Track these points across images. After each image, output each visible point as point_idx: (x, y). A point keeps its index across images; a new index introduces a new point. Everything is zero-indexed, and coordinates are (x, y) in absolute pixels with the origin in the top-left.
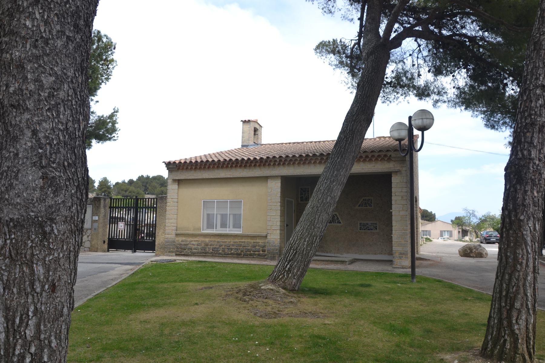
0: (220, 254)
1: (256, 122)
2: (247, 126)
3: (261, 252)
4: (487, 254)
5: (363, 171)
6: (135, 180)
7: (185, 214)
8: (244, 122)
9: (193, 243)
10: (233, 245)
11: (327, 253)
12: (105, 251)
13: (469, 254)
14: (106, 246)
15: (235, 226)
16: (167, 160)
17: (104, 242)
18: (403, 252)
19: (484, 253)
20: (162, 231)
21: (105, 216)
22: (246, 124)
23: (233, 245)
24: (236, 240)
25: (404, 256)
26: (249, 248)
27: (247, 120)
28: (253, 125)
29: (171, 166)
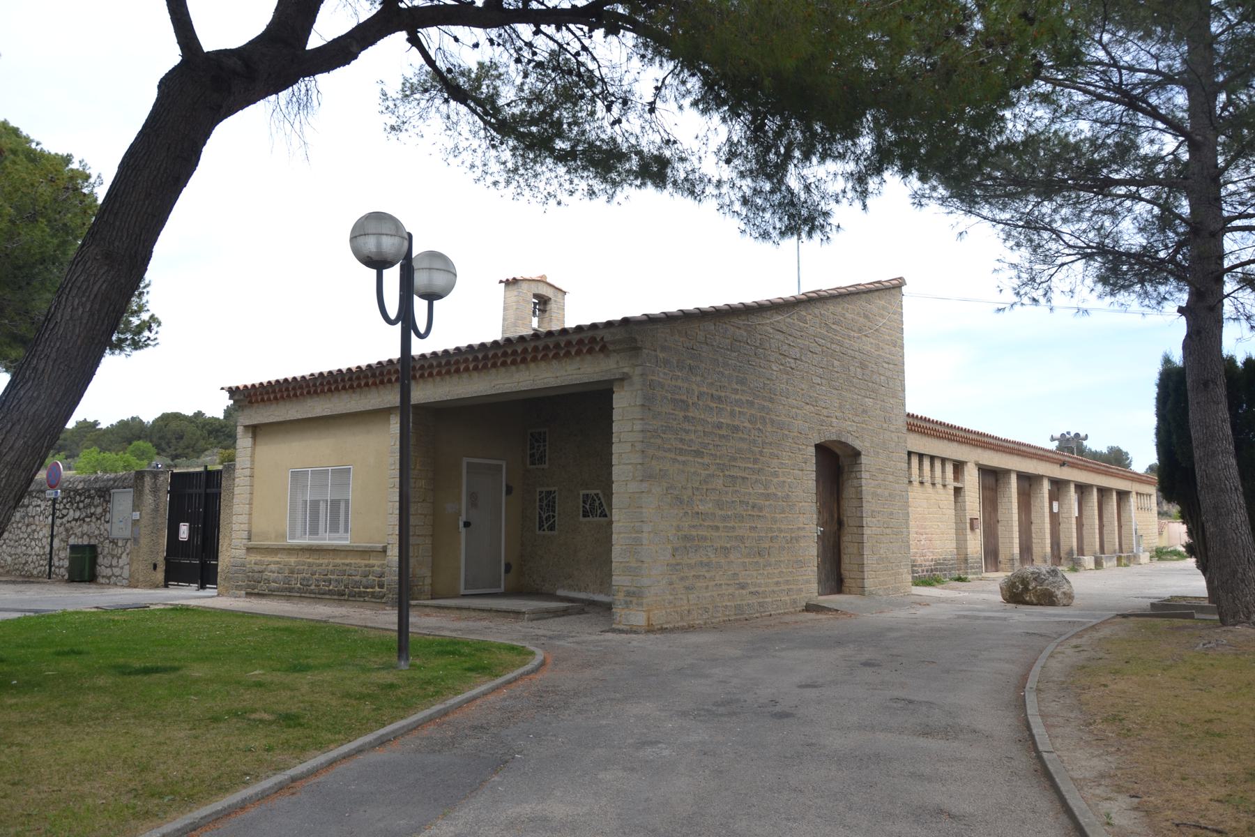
0: (312, 592)
1: (542, 281)
2: (513, 292)
3: (377, 589)
4: (1069, 596)
5: (559, 382)
6: (104, 425)
7: (267, 502)
8: (511, 283)
9: (273, 567)
10: (333, 573)
11: (580, 590)
12: (157, 587)
13: (1021, 594)
14: (160, 575)
15: (334, 528)
16: (233, 385)
17: (155, 567)
18: (632, 589)
19: (1059, 593)
20: (227, 541)
21: (156, 510)
22: (510, 287)
23: (333, 573)
24: (338, 561)
25: (635, 600)
26: (358, 578)
27: (510, 278)
28: (527, 292)
29: (244, 397)
